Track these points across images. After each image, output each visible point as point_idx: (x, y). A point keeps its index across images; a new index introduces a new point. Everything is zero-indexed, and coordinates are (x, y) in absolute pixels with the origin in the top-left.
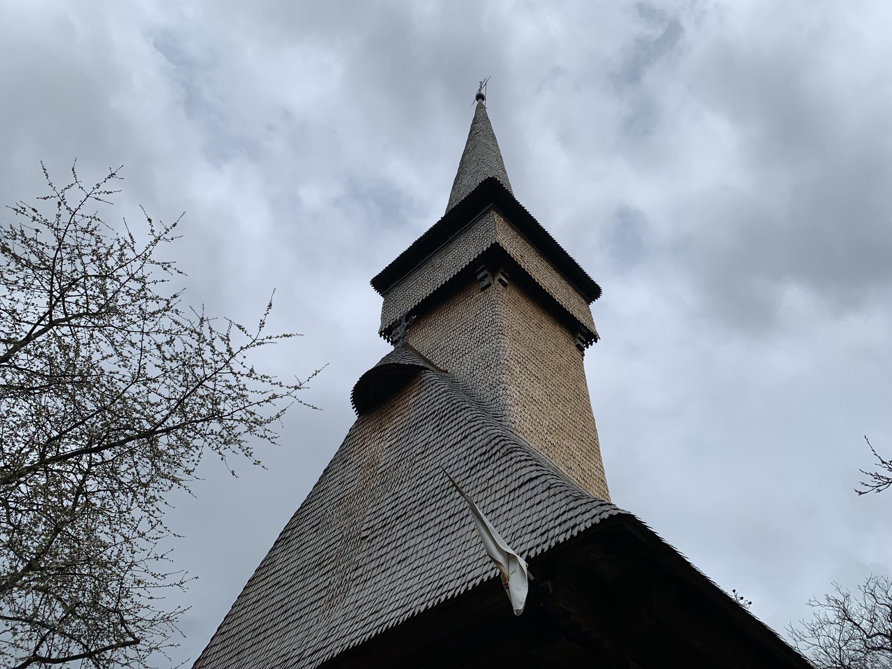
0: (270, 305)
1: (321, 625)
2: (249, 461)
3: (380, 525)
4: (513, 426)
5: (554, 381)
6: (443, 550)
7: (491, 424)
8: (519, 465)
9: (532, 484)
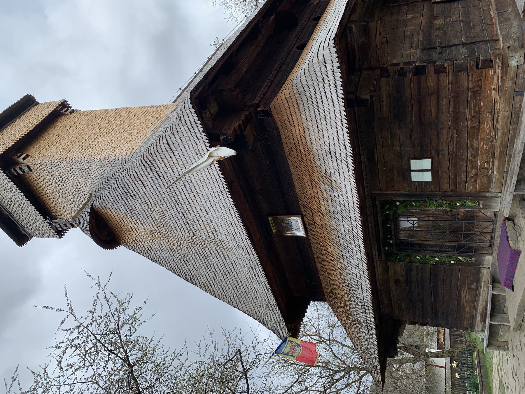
0: (45, 307)
1: (236, 252)
2: (144, 307)
3: (188, 226)
4: (128, 154)
5: (97, 129)
6: (203, 191)
7: (133, 165)
8: (159, 150)
9: (171, 143)
